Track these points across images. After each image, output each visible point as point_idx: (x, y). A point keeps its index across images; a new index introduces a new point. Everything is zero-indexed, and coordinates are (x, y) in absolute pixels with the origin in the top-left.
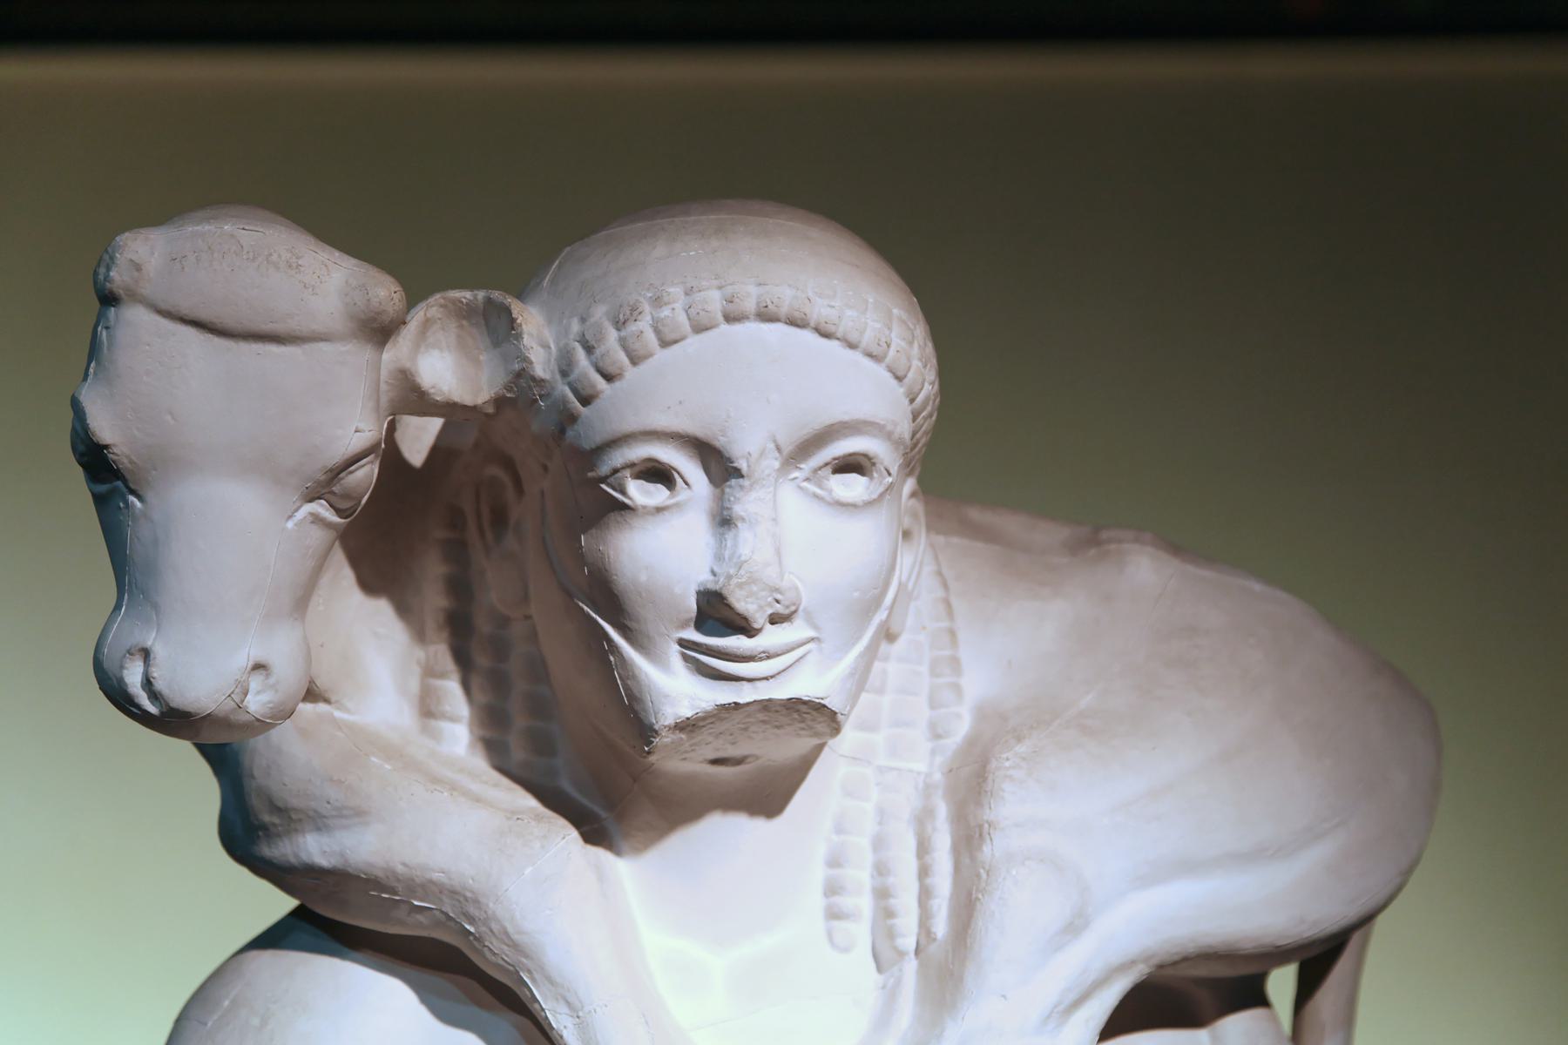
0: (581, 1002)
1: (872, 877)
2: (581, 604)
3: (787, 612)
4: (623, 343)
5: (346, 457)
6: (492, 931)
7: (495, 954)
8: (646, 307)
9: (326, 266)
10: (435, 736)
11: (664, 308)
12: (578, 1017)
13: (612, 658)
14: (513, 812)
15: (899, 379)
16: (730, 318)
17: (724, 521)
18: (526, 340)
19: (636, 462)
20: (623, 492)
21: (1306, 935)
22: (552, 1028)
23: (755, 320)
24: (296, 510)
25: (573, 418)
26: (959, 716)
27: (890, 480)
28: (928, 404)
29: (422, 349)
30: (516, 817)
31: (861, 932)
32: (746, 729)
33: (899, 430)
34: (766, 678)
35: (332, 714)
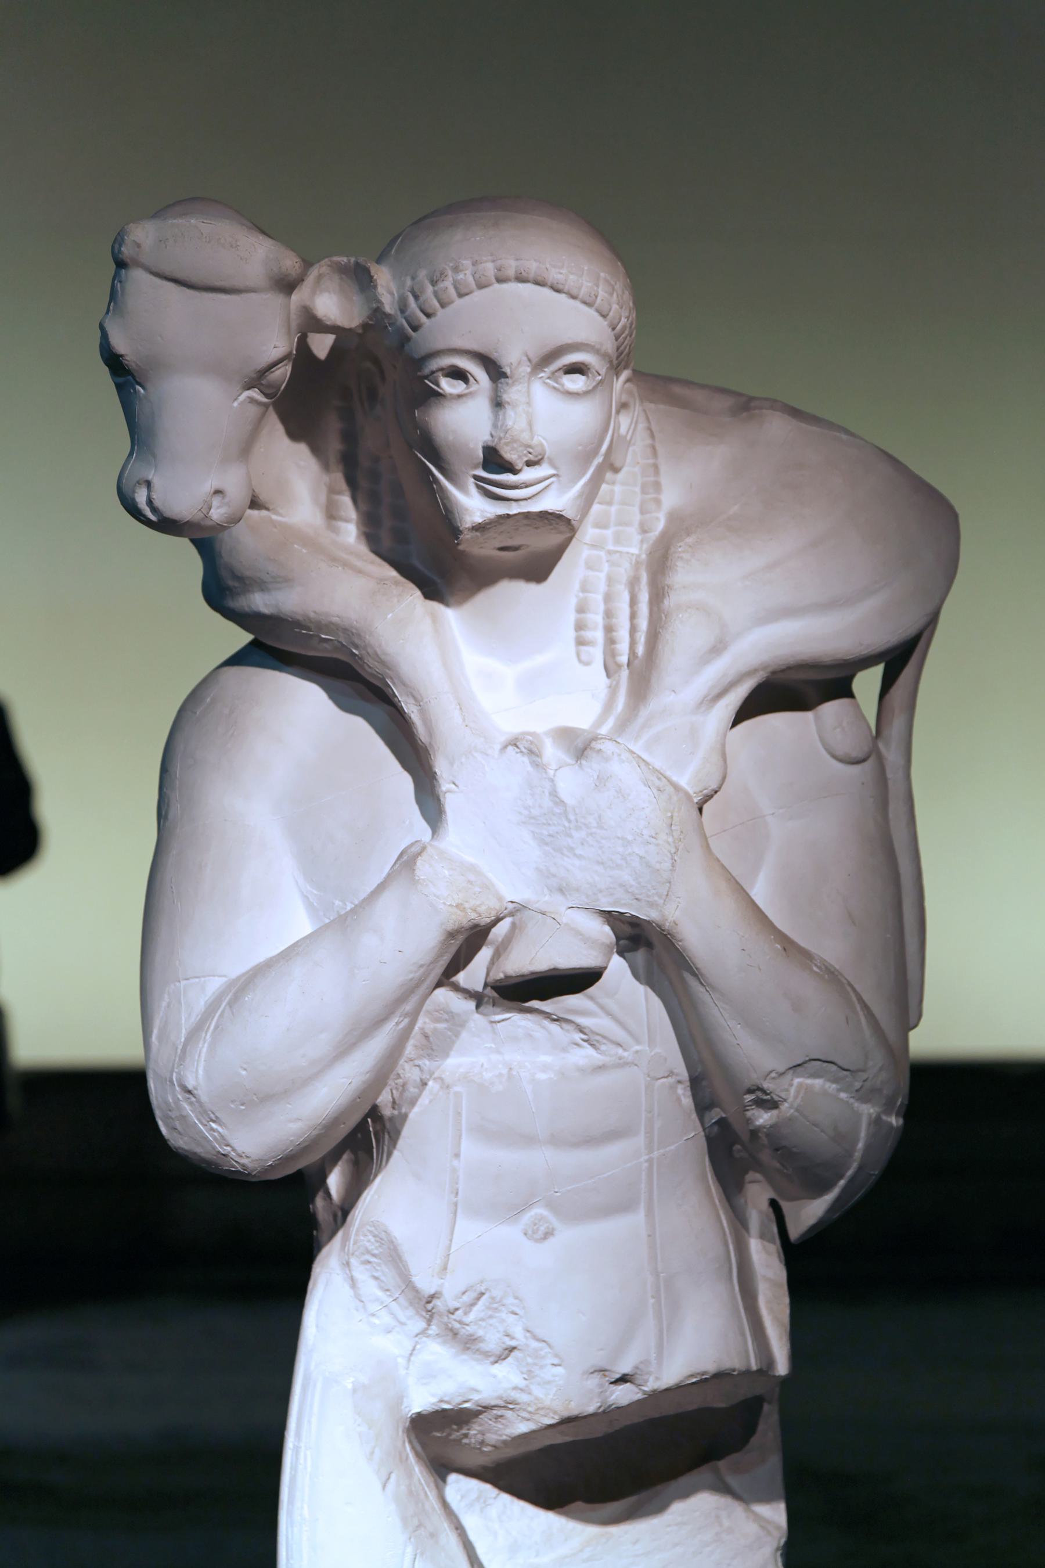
0: (421, 696)
1: (604, 619)
2: (416, 452)
3: (536, 459)
4: (436, 294)
5: (268, 363)
6: (368, 653)
7: (370, 667)
8: (450, 273)
9: (254, 246)
10: (336, 531)
11: (460, 273)
12: (420, 706)
13: (435, 486)
14: (381, 580)
15: (604, 316)
16: (500, 280)
17: (498, 404)
18: (380, 290)
19: (445, 367)
20: (438, 385)
21: (863, 653)
22: (405, 713)
23: (514, 281)
24: (239, 395)
25: (408, 339)
26: (658, 519)
27: (600, 378)
28: (625, 330)
29: (318, 292)
30: (382, 583)
31: (597, 653)
32: (517, 529)
33: (604, 348)
34: (525, 499)
35: (271, 518)
